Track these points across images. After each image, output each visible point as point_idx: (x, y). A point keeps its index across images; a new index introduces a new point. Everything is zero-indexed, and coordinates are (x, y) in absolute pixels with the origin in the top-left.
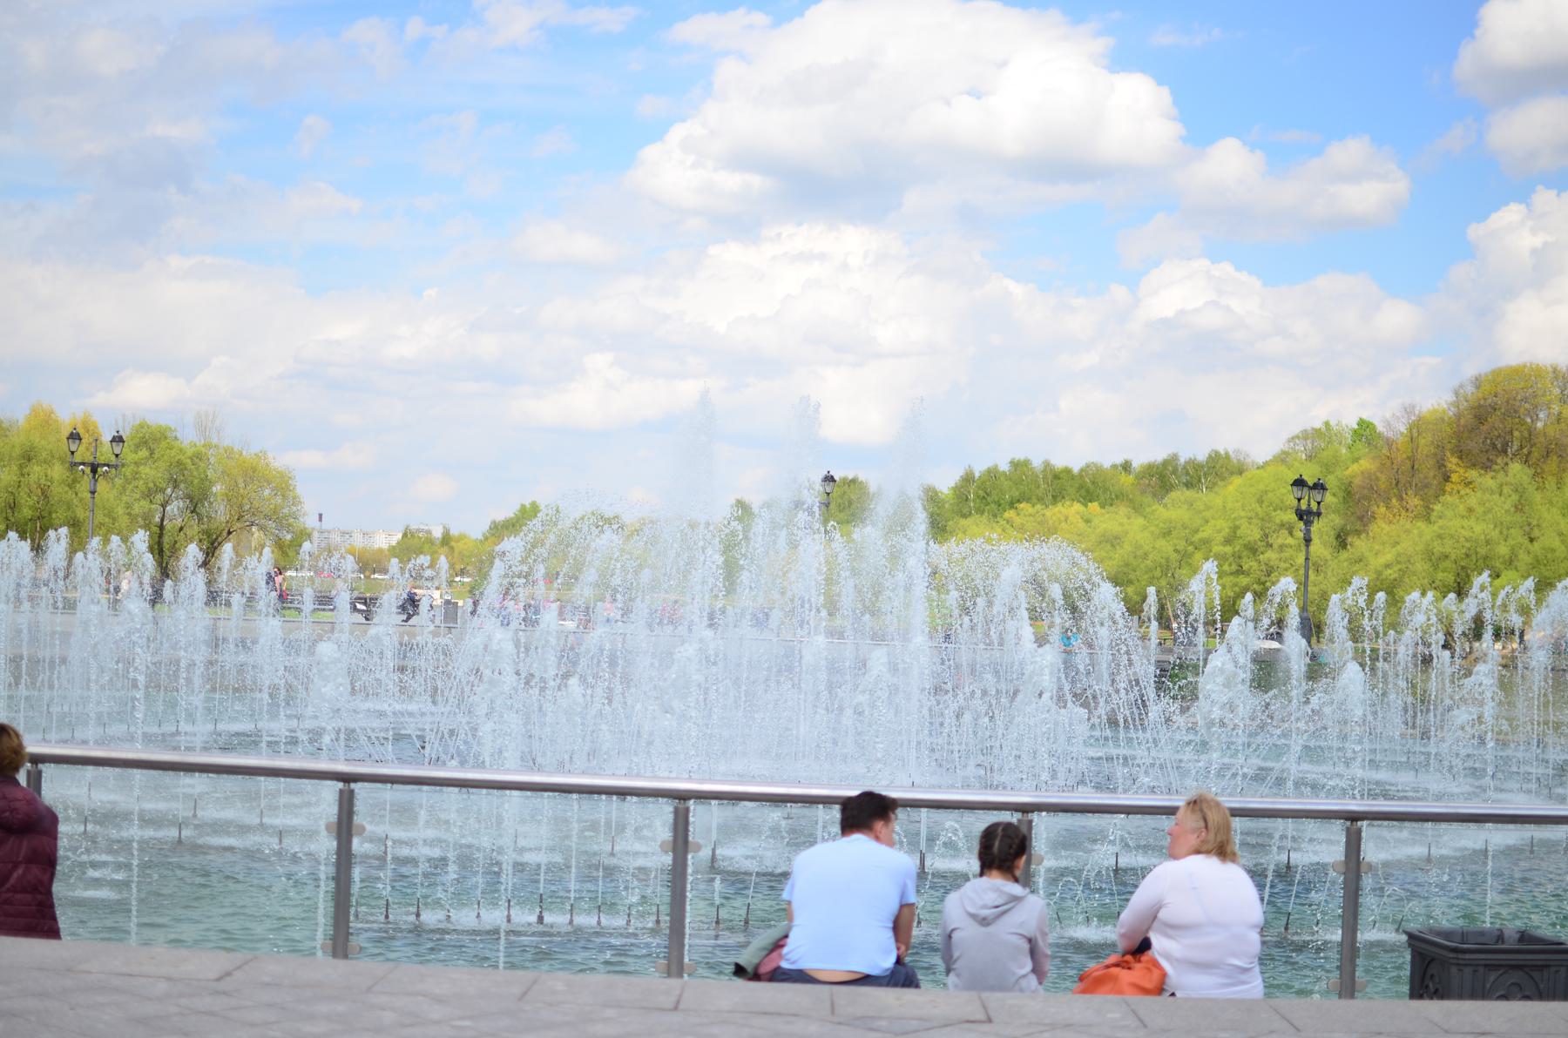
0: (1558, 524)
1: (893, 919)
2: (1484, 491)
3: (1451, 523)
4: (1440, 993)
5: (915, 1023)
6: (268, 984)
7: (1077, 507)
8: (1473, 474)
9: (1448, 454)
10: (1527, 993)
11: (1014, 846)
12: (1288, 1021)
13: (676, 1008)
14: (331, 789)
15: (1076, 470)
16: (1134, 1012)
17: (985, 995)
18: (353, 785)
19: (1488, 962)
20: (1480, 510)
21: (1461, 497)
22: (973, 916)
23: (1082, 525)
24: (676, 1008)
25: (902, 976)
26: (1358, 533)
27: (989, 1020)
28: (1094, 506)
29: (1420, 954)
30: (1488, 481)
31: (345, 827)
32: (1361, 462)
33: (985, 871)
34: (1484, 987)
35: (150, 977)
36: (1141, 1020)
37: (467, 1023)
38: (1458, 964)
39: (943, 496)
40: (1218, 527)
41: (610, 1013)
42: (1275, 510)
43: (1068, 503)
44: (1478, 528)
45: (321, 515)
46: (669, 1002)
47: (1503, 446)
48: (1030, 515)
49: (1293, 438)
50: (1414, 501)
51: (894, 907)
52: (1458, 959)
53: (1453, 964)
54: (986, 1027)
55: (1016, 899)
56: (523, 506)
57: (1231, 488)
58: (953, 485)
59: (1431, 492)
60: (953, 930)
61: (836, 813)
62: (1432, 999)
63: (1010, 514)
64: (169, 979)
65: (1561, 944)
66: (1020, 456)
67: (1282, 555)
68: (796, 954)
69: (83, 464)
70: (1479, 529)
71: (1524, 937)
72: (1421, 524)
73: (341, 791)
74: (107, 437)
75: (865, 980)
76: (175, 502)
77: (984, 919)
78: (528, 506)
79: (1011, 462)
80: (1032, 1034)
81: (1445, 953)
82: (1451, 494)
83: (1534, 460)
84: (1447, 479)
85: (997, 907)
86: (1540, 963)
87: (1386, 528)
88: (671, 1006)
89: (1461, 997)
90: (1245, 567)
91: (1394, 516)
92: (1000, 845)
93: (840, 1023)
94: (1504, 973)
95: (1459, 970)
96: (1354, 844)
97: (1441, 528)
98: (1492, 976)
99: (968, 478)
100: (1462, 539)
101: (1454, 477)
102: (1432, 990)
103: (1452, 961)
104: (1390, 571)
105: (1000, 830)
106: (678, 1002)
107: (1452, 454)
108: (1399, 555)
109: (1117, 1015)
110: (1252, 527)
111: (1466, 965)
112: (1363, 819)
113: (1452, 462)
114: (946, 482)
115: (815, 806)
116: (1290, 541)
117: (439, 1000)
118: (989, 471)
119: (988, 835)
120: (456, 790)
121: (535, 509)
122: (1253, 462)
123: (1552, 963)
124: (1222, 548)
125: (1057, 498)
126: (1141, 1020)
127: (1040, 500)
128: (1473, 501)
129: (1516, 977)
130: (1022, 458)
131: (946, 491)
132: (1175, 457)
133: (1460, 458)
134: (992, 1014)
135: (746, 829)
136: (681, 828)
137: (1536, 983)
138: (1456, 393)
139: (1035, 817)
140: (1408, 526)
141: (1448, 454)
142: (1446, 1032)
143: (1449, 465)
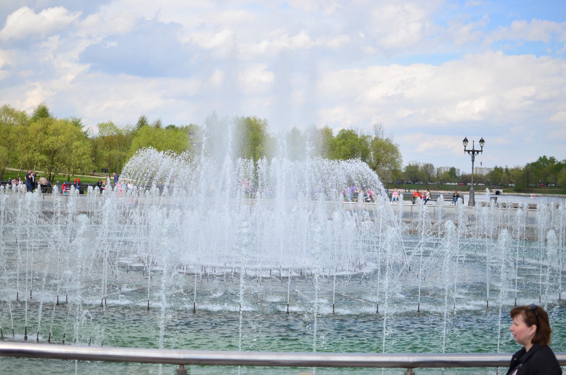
45: (481, 163)
56: (541, 158)
78: (542, 157)
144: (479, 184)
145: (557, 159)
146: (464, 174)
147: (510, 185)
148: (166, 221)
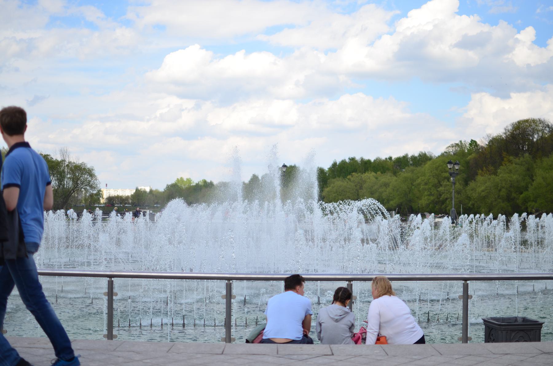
1: (303, 320)
4: (494, 341)
5: (306, 356)
7: (373, 174)
8: (511, 158)
9: (503, 151)
13: (222, 354)
14: (105, 280)
15: (372, 160)
17: (332, 346)
18: (113, 279)
19: (512, 329)
22: (332, 318)
24: (222, 354)
25: (306, 340)
27: (333, 354)
31: (111, 293)
35: (37, 348)
36: (386, 353)
37: (148, 361)
38: (501, 330)
39: (326, 171)
40: (423, 179)
41: (199, 356)
43: (370, 172)
44: (514, 177)
45: (106, 184)
46: (220, 351)
48: (356, 177)
49: (448, 147)
50: (491, 168)
52: (501, 328)
53: (499, 330)
54: (332, 357)
55: (347, 313)
56: (178, 179)
57: (427, 165)
61: (283, 283)
62: (492, 342)
65: (537, 322)
66: (352, 156)
67: (446, 188)
71: (524, 319)
72: (493, 176)
75: (293, 342)
77: (336, 320)
78: (180, 179)
80: (348, 359)
81: (497, 326)
84: (503, 160)
85: (340, 316)
86: (530, 329)
88: (221, 353)
89: (502, 341)
92: (341, 295)
93: (280, 357)
94: (517, 333)
95: (501, 332)
97: (501, 177)
99: (335, 165)
100: (509, 181)
101: (505, 159)
102: (493, 340)
103: (499, 329)
104: (483, 193)
105: (343, 290)
106: (223, 351)
112: (469, 280)
113: (504, 154)
114: (326, 167)
115: (243, 281)
116: (448, 183)
117: (138, 353)
118: (342, 161)
122: (434, 156)
126: (386, 353)
127: (360, 172)
131: (327, 170)
132: (407, 155)
134: (334, 352)
135: (190, 290)
138: (505, 129)
139: (353, 283)
141: (503, 151)
143: (503, 155)
144: (126, 205)
145: (193, 180)
146: (111, 196)
147: (155, 205)
148: (409, 224)
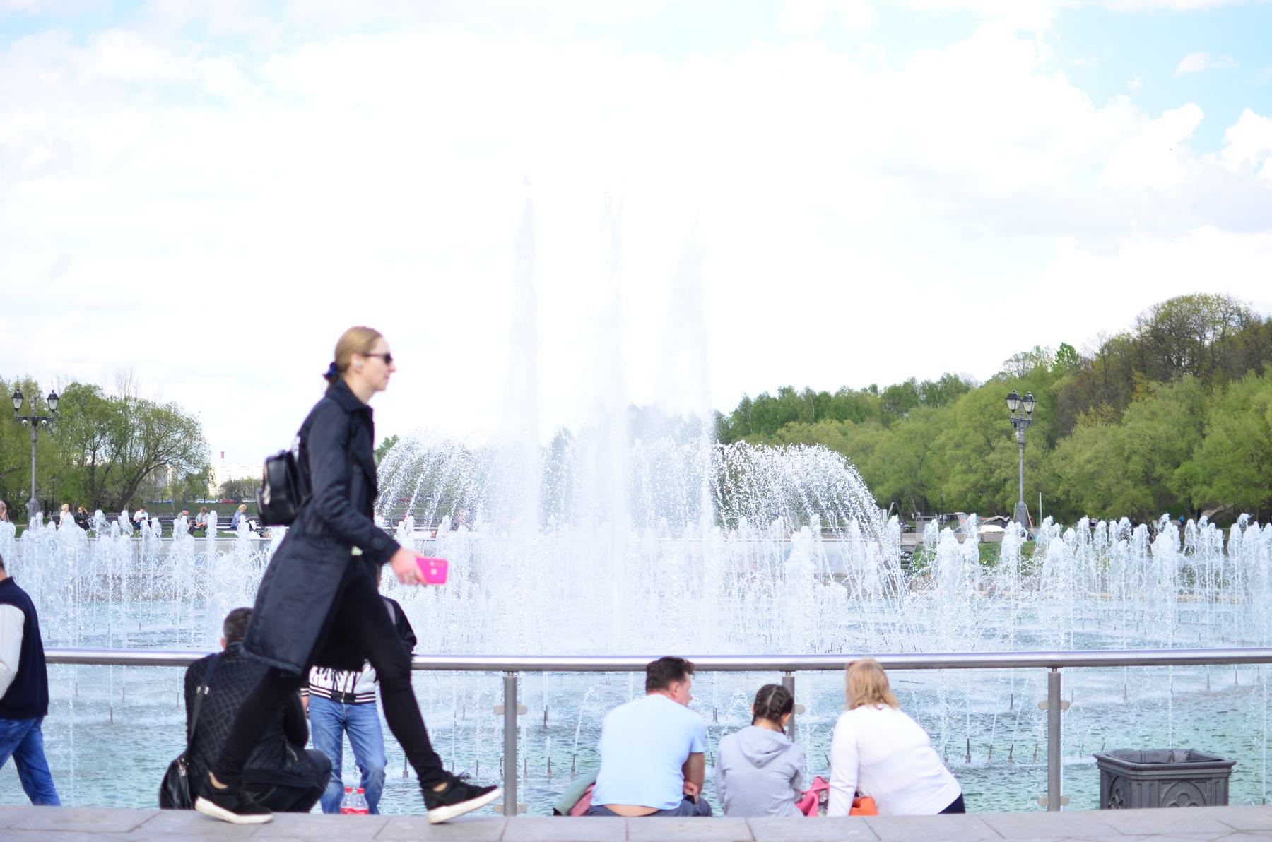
0: (1225, 422)
2: (1164, 397)
3: (1139, 425)
6: (170, 834)
7: (836, 423)
8: (1153, 385)
9: (1133, 369)
10: (1194, 801)
11: (784, 703)
12: (996, 831)
16: (871, 828)
19: (1161, 777)
20: (1162, 413)
21: (1145, 404)
22: (749, 759)
23: (839, 436)
26: (1064, 435)
28: (848, 422)
29: (1108, 773)
30: (1166, 390)
32: (1064, 378)
33: (757, 718)
34: (1159, 797)
38: (1138, 780)
40: (951, 435)
42: (995, 420)
45: (223, 453)
47: (1177, 362)
49: (1007, 361)
50: (1107, 408)
51: (683, 754)
57: (959, 403)
58: (734, 410)
59: (1121, 400)
60: (727, 769)
61: (643, 676)
62: (1118, 808)
63: (781, 431)
64: (90, 832)
67: (1004, 455)
68: (601, 796)
69: (26, 418)
70: (1162, 428)
71: (1191, 756)
73: (1050, 675)
74: (45, 395)
75: (659, 812)
76: (103, 447)
77: (759, 762)
79: (779, 390)
82: (1137, 401)
83: (1203, 372)
85: (768, 753)
86: (1203, 776)
87: (1086, 431)
89: (1141, 806)
90: (974, 467)
91: (1092, 420)
95: (1139, 785)
96: (1054, 685)
98: (1166, 788)
99: (746, 404)
100: (1148, 438)
101: (1139, 388)
103: (1132, 778)
107: (1136, 369)
108: (1097, 452)
109: (857, 832)
110: (978, 434)
111: (1143, 780)
114: (729, 408)
118: (761, 397)
119: (764, 693)
120: (483, 673)
121: (395, 439)
123: (1213, 776)
124: (953, 452)
125: (818, 417)
127: (806, 419)
128: (1155, 405)
129: (1184, 788)
130: (787, 386)
132: (913, 380)
133: (1144, 371)
136: (510, 694)
137: (1201, 792)
138: (1139, 320)
140: (1104, 428)
142: (1123, 834)
